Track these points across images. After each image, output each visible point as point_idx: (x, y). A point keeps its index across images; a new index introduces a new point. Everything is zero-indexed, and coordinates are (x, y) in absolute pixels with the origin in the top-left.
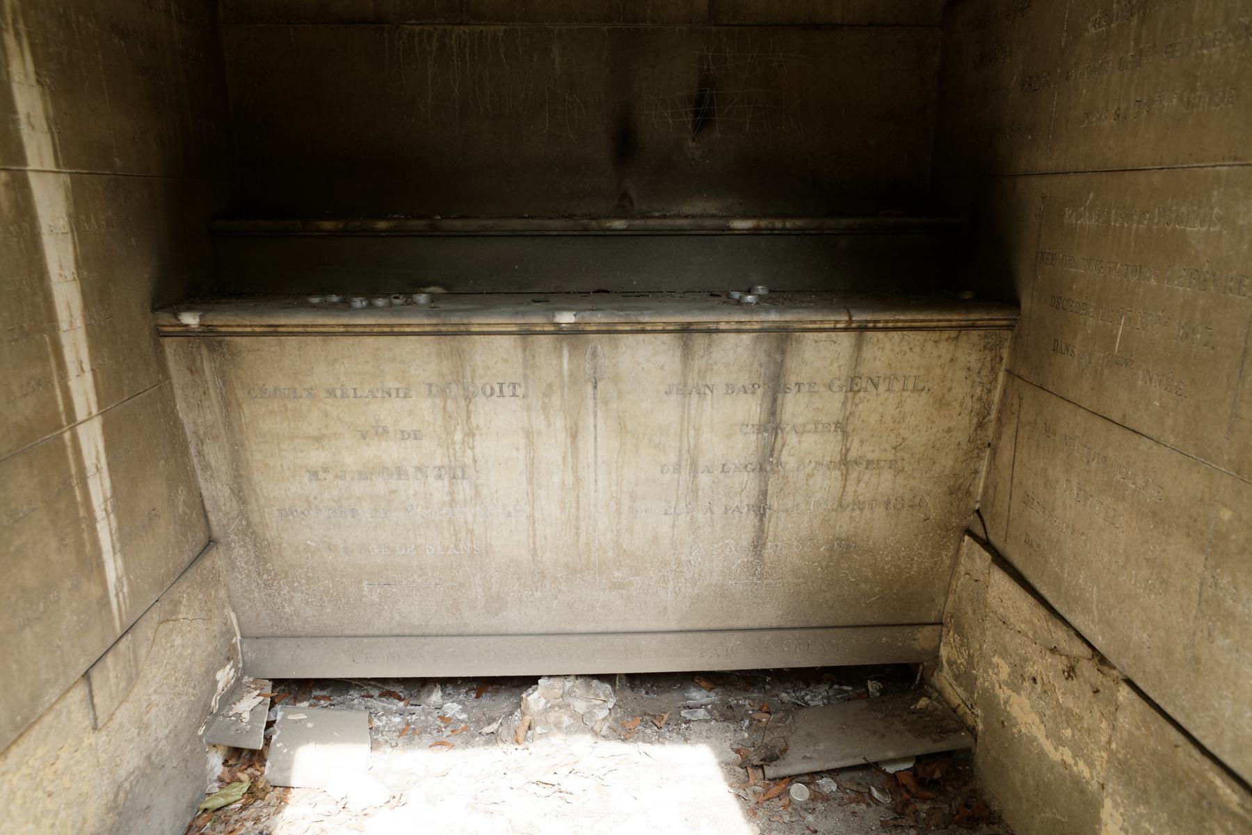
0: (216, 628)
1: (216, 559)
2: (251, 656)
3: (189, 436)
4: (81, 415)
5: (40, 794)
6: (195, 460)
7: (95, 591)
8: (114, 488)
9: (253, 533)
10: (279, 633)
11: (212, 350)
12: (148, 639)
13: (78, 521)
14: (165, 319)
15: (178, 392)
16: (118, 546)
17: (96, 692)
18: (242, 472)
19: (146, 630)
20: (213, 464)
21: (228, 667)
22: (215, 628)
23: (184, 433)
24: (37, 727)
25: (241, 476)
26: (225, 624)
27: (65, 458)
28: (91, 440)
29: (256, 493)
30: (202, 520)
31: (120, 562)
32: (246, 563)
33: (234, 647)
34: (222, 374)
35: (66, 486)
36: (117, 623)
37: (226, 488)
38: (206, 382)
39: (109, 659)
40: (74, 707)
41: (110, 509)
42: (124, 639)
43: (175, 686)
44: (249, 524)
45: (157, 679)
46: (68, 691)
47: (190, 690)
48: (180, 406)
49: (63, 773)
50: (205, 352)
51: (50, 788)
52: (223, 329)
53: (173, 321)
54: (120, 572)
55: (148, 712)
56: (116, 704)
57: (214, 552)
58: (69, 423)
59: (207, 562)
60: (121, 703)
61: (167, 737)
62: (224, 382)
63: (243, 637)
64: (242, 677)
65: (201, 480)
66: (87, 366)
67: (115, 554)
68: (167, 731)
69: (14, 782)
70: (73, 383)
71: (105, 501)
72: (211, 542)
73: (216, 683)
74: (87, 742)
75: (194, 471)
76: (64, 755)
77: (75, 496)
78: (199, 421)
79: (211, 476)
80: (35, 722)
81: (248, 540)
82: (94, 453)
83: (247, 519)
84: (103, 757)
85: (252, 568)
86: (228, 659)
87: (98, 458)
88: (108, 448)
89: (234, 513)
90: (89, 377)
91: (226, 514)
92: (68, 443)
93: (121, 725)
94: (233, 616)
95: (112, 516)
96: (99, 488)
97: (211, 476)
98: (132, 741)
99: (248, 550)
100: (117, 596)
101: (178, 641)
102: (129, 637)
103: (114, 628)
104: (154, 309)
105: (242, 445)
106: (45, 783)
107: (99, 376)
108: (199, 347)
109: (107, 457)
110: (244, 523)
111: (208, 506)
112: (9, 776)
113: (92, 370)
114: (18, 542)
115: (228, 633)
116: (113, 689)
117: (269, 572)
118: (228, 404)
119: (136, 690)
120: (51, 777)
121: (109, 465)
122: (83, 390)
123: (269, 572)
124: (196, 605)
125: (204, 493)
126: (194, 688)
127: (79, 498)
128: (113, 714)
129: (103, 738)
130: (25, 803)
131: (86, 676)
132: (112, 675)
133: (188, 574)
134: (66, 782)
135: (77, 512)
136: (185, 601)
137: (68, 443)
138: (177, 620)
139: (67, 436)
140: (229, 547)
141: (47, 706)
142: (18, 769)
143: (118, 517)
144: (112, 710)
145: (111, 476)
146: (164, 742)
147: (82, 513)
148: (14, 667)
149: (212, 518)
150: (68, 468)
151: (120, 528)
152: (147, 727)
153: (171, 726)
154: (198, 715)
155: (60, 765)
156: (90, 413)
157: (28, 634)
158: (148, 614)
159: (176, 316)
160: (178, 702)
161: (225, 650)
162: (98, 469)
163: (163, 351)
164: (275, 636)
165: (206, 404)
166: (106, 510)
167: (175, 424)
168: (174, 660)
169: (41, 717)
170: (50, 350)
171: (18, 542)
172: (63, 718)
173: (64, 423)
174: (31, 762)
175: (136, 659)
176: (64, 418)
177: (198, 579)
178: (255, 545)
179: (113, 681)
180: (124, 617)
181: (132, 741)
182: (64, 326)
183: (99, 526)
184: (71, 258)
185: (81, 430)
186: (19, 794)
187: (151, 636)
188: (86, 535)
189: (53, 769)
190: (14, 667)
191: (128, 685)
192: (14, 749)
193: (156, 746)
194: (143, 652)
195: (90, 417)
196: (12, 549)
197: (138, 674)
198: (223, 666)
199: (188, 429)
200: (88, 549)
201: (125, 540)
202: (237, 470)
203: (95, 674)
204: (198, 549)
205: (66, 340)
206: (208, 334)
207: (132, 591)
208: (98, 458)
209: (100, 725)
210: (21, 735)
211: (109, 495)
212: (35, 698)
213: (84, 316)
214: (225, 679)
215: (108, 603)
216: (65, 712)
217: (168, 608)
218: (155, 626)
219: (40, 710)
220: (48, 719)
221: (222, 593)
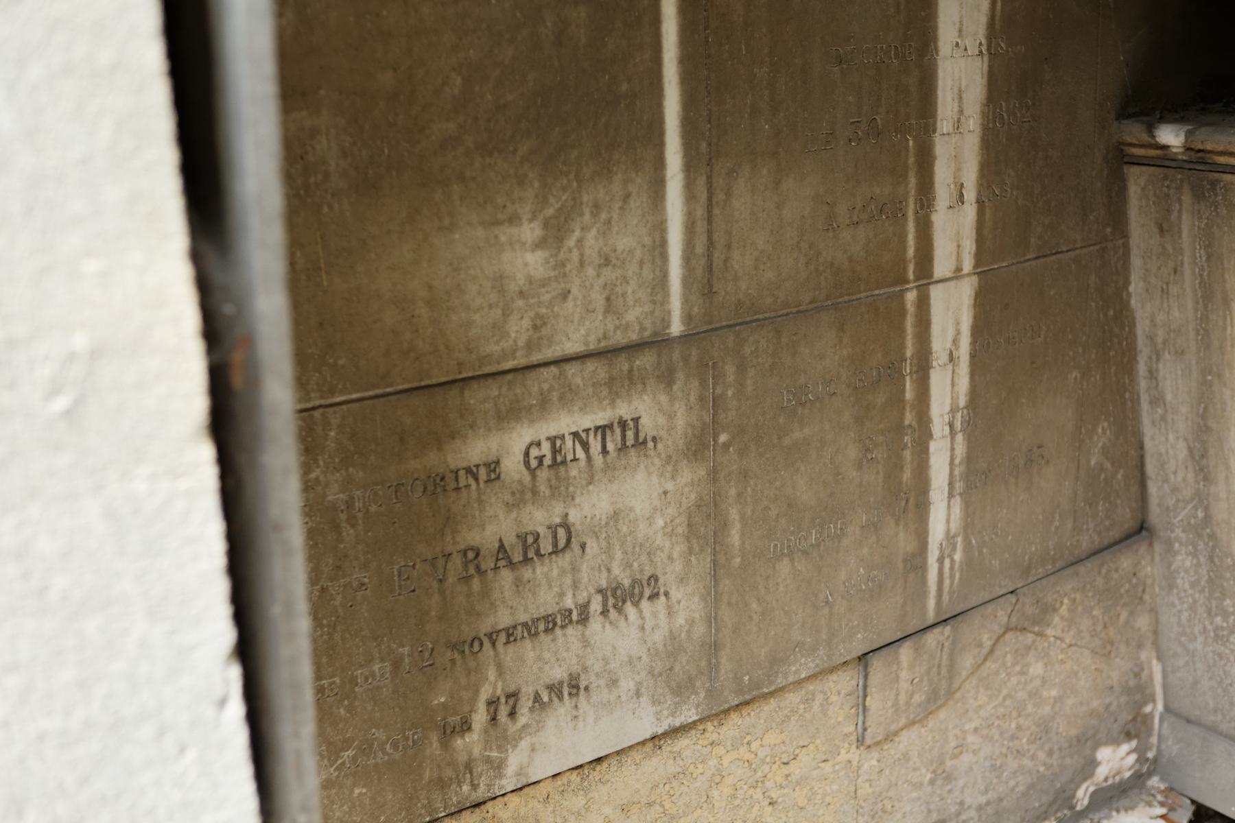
0: (1118, 670)
1: (1144, 563)
2: (1172, 748)
3: (1141, 342)
4: (942, 266)
5: (758, 794)
6: (1143, 384)
7: (905, 543)
8: (973, 392)
9: (1212, 536)
10: (1224, 727)
11: (1199, 196)
12: (980, 645)
13: (899, 429)
14: (1133, 132)
15: (1136, 261)
16: (959, 486)
17: (872, 690)
18: (1212, 424)
19: (981, 630)
20: (1169, 397)
21: (1125, 748)
22: (1115, 675)
23: (1132, 332)
24: (773, 703)
25: (1208, 429)
26: (1137, 675)
27: (901, 329)
28: (951, 312)
29: (1228, 467)
30: (1134, 489)
31: (957, 510)
32: (1192, 585)
33: (1147, 720)
34: (1208, 240)
35: (893, 373)
36: (931, 603)
37: (1182, 445)
38: (1180, 251)
39: (905, 652)
40: (834, 698)
41: (958, 425)
42: (937, 630)
43: (1013, 738)
44: (1208, 519)
45: (983, 713)
46: (833, 670)
47: (1042, 755)
48: (1136, 286)
49: (798, 783)
50: (1187, 198)
51: (774, 794)
52: (1222, 160)
53: (1145, 138)
54: (955, 525)
55: (955, 757)
56: (902, 722)
57: (1143, 548)
58: (917, 279)
59: (1125, 562)
60: (913, 723)
61: (980, 808)
62: (1209, 257)
63: (1167, 708)
64: (1150, 774)
65: (1146, 421)
66: (970, 195)
67: (951, 496)
68: (983, 799)
69: (725, 763)
70: (941, 218)
71: (954, 410)
72: (1141, 529)
73: (1093, 764)
74: (843, 757)
75: (1136, 401)
76: (805, 759)
77: (903, 391)
78: (1160, 318)
79: (1163, 418)
80: (772, 694)
81: (1201, 546)
82: (951, 333)
83: (1206, 509)
84: (865, 789)
85: (1201, 599)
86: (1128, 736)
87: (955, 342)
88: (978, 330)
89: (1188, 492)
90: (969, 212)
91: (1175, 490)
92: (910, 308)
93: (906, 757)
94: (1157, 668)
95: (960, 437)
96: (948, 389)
97: (1163, 418)
98: (918, 786)
99: (1198, 565)
100: (941, 560)
101: (1037, 669)
102: (947, 630)
103: (924, 608)
104: (1122, 115)
105: (1220, 376)
106: (768, 784)
107: (988, 214)
108: (1179, 189)
109: (973, 343)
110: (1200, 514)
111: (1150, 468)
112: (720, 750)
113: (979, 202)
114: (797, 435)
115: (1138, 692)
116: (903, 698)
117: (1226, 615)
118: (1209, 295)
119: (942, 714)
120: (779, 779)
121: (973, 356)
122: (954, 232)
123: (1226, 615)
124: (1085, 624)
125: (1148, 444)
126: (1050, 753)
127: (909, 395)
128: (896, 734)
129: (871, 762)
130: (734, 797)
131: (863, 658)
132: (904, 675)
133: (1081, 569)
134: (800, 796)
135: (902, 418)
136: (1064, 610)
137: (910, 308)
138: (1040, 634)
139: (911, 296)
140: (1169, 550)
141: (791, 679)
142: (735, 748)
143: (969, 439)
144: (894, 727)
145: (972, 375)
146: (973, 813)
147: (909, 418)
148: (754, 606)
149: (1153, 489)
150: (902, 346)
151: (970, 458)
152: (949, 778)
153: (991, 795)
154: (1045, 799)
155: (795, 769)
156: (959, 269)
157: (784, 567)
158: (989, 608)
159: (1150, 129)
160: (1013, 764)
161: (1126, 716)
162: (951, 358)
163: (1123, 190)
164: (1213, 729)
165: (1174, 290)
166: (951, 425)
167: (1121, 314)
168: (1022, 695)
169: (782, 689)
170: (911, 160)
171: (797, 435)
172: (816, 706)
173: (911, 276)
174: (754, 746)
175: (952, 667)
176: (911, 268)
177: (1100, 581)
178: (1211, 559)
179: (904, 685)
180: (946, 597)
181: (918, 786)
182: (944, 123)
183: (933, 446)
184: (983, 20)
185: (937, 294)
186: (729, 780)
187: (988, 644)
188: (907, 454)
189: (785, 770)
190: (754, 606)
191: (928, 701)
192: (734, 717)
193: (958, 814)
194: (967, 662)
195: (958, 274)
196: (787, 441)
197: (950, 694)
198: (1116, 742)
199: (1142, 327)
200: (907, 475)
201: (975, 479)
202: (1204, 417)
203: (876, 663)
204: (1115, 534)
205: (942, 149)
206: (1197, 164)
207: (968, 562)
208: (955, 342)
209: (868, 741)
210: (747, 703)
211: (962, 402)
212: (777, 661)
213: (984, 115)
214: (1115, 765)
215: (922, 568)
216: (819, 698)
217: (1030, 610)
218: (998, 630)
219: (780, 681)
220: (793, 698)
221: (1143, 622)
